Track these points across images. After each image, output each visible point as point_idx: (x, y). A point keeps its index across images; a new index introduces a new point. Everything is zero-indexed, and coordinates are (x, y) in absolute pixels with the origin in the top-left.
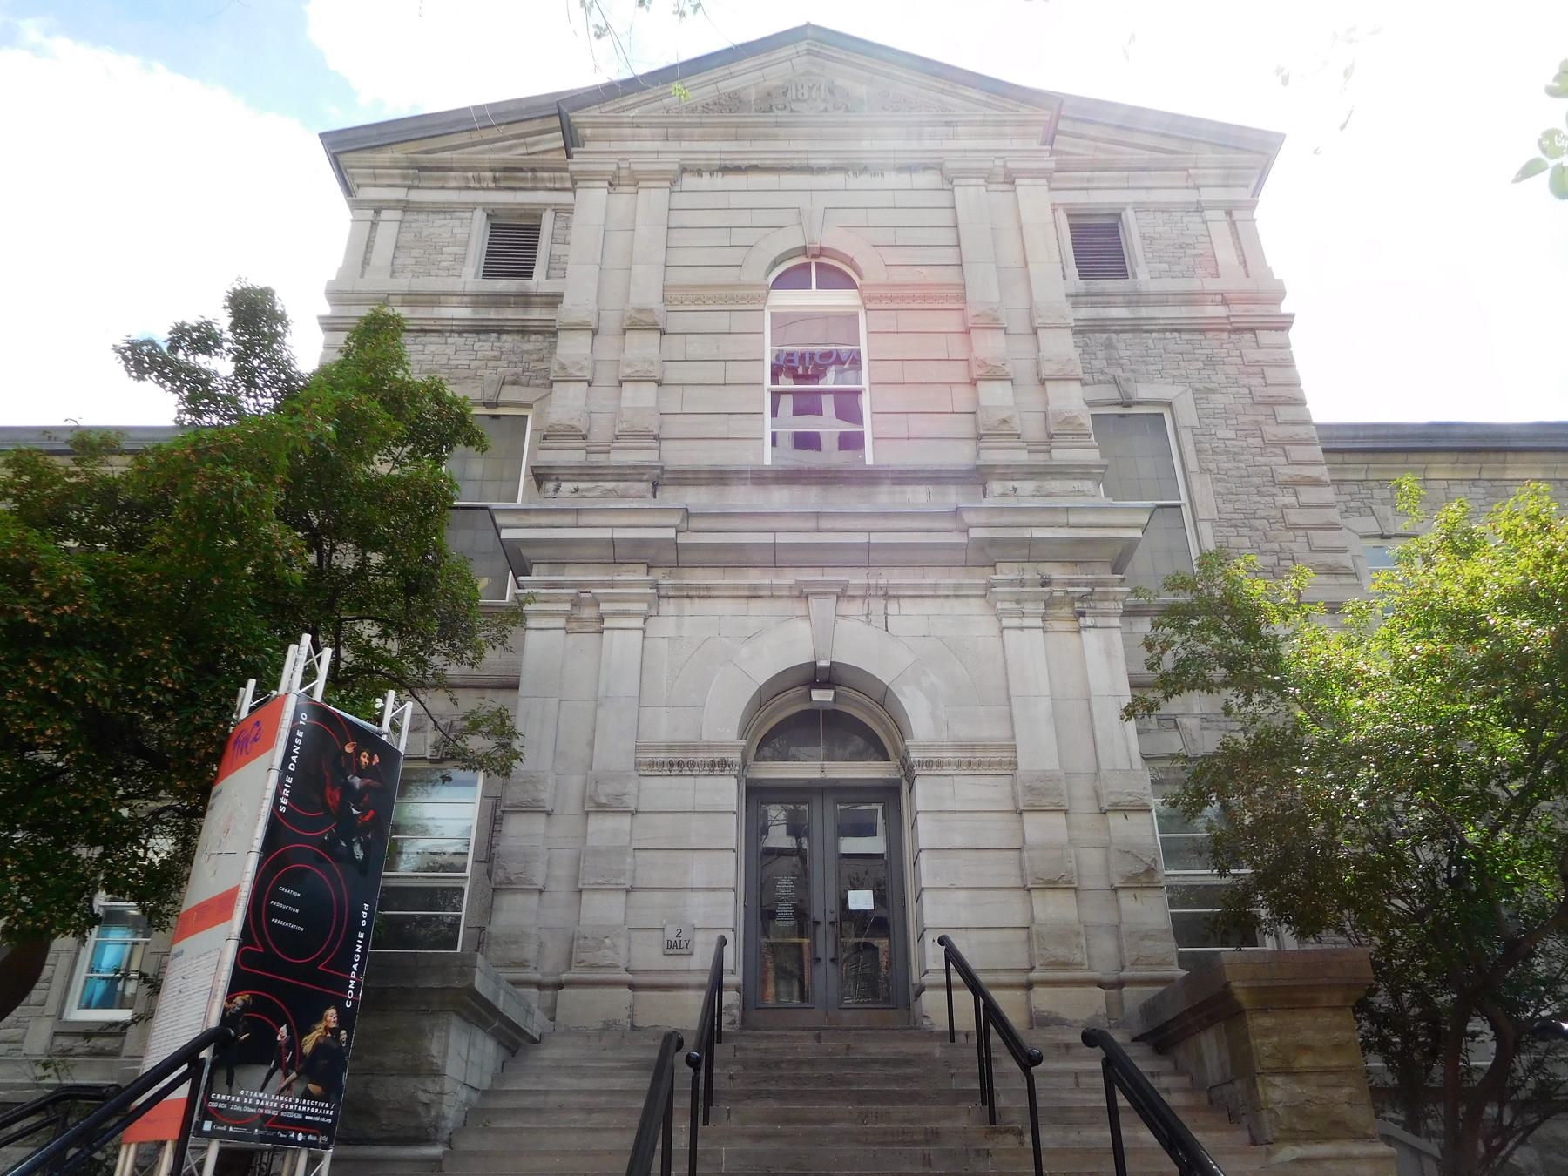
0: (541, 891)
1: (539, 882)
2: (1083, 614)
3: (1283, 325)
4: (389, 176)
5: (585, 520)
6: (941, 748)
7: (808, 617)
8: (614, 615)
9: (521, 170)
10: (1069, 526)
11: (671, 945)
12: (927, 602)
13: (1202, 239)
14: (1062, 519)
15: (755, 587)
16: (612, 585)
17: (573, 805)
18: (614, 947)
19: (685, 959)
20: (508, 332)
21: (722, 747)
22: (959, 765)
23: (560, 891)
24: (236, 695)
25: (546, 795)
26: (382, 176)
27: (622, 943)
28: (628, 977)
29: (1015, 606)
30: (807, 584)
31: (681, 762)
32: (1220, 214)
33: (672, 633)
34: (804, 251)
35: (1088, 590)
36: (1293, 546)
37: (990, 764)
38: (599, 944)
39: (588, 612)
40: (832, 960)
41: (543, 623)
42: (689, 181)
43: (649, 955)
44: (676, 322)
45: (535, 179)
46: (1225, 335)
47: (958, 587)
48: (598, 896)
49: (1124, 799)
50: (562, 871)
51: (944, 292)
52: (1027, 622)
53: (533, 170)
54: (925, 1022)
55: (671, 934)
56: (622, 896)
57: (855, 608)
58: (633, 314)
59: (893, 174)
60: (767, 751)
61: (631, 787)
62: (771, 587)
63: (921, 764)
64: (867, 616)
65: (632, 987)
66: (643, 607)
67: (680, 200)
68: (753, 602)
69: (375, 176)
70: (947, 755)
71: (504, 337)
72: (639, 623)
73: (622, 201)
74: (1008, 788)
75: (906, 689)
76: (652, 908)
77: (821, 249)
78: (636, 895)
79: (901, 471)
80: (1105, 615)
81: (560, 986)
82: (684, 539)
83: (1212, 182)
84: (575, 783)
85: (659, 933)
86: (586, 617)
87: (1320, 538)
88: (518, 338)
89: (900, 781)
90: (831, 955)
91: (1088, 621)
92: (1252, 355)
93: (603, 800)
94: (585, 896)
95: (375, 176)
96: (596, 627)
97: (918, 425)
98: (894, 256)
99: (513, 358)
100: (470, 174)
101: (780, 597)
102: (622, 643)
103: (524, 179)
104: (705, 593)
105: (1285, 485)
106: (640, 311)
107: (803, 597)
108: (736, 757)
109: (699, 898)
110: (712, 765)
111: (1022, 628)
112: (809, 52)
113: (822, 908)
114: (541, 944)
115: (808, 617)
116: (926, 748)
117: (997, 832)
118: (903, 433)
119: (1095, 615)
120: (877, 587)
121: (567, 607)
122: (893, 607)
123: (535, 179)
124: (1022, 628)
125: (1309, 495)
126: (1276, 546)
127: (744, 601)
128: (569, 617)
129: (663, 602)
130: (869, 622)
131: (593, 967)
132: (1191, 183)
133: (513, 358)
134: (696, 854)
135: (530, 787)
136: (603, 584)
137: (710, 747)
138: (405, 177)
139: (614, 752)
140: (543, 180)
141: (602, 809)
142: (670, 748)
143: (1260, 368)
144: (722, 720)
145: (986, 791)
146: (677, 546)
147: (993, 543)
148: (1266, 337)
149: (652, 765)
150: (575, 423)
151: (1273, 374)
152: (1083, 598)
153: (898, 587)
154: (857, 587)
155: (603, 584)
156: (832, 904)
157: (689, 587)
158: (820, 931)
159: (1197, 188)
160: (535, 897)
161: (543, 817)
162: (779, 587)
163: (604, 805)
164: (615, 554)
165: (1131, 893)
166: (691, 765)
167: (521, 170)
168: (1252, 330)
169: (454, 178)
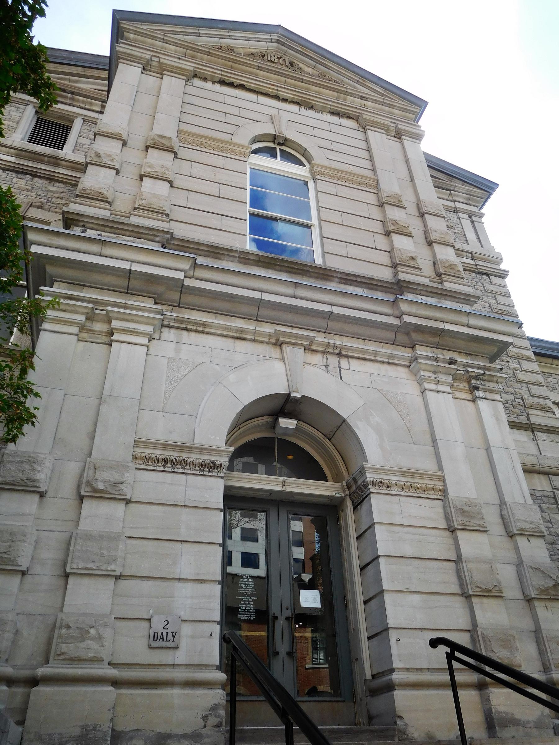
0: (24, 573)
1: (24, 563)
2: (477, 388)
3: (503, 275)
5: (108, 251)
6: (390, 472)
7: (283, 360)
8: (124, 331)
10: (468, 326)
11: (157, 637)
12: (368, 364)
13: (458, 226)
14: (464, 320)
15: (242, 331)
16: (125, 306)
17: (68, 489)
18: (99, 638)
19: (171, 652)
20: (40, 177)
21: (213, 451)
22: (403, 488)
23: (45, 576)
25: (42, 476)
27: (107, 633)
28: (113, 672)
29: (433, 375)
30: (284, 334)
31: (174, 460)
32: (466, 216)
33: (172, 354)
34: (274, 138)
35: (481, 372)
36: (521, 391)
37: (426, 490)
38: (83, 634)
39: (99, 326)
40: (289, 654)
41: (57, 328)
42: (197, 82)
43: (130, 646)
44: (182, 153)
46: (474, 274)
47: (392, 356)
48: (86, 581)
49: (527, 526)
50: (50, 554)
51: (365, 181)
52: (441, 388)
53: (72, 93)
54: (399, 722)
55: (158, 625)
56: (112, 581)
57: (317, 359)
58: (156, 138)
59: (329, 115)
60: (238, 463)
61: (129, 476)
62: (255, 333)
63: (374, 483)
64: (326, 366)
65: (116, 683)
66: (150, 329)
67: (189, 89)
68: (239, 343)
70: (394, 478)
71: (36, 179)
72: (145, 341)
73: (151, 80)
74: (441, 510)
75: (360, 424)
76: (140, 597)
77: (286, 139)
78: (123, 583)
79: (347, 274)
80: (491, 391)
81: (34, 682)
82: (188, 282)
83: (461, 200)
84: (72, 469)
85: (146, 624)
86: (101, 330)
87: (535, 390)
88: (46, 182)
89: (342, 501)
90: (287, 649)
91: (479, 394)
92: (489, 287)
93: (101, 486)
94: (71, 580)
96: (105, 339)
97: (353, 251)
98: (331, 155)
99: (41, 193)
101: (260, 342)
102: (128, 355)
104: (201, 329)
105: (513, 357)
106: (162, 137)
107: (279, 344)
108: (225, 460)
109: (187, 589)
110: (203, 465)
111: (438, 392)
112: (278, 42)
113: (278, 607)
114: (17, 632)
115: (283, 360)
116: (376, 470)
117: (438, 545)
118: (344, 253)
119: (485, 390)
120: (335, 347)
121: (83, 318)
122: (344, 363)
123: (72, 99)
124: (438, 392)
125: (526, 365)
126: (512, 390)
127: (231, 340)
128: (82, 328)
129: (165, 330)
130: (328, 371)
131: (74, 660)
132: (451, 198)
133: (41, 193)
134: (185, 545)
135: (27, 466)
136: (116, 305)
137: (202, 450)
139: (113, 445)
140: (78, 101)
141: (98, 495)
142: (166, 446)
143: (494, 295)
144: (213, 432)
145: (429, 512)
146: (182, 288)
147: (418, 328)
148: (495, 280)
149: (147, 460)
150: (104, 192)
151: (500, 299)
152: (477, 378)
153: (349, 348)
154: (320, 344)
155: (116, 305)
156: (287, 602)
157: (188, 321)
158: (278, 625)
159: (454, 201)
160: (17, 579)
161: (36, 497)
162: (261, 334)
163: (101, 491)
164: (131, 284)
165: (542, 604)
166: (183, 463)
167: (64, 91)
168: (487, 275)
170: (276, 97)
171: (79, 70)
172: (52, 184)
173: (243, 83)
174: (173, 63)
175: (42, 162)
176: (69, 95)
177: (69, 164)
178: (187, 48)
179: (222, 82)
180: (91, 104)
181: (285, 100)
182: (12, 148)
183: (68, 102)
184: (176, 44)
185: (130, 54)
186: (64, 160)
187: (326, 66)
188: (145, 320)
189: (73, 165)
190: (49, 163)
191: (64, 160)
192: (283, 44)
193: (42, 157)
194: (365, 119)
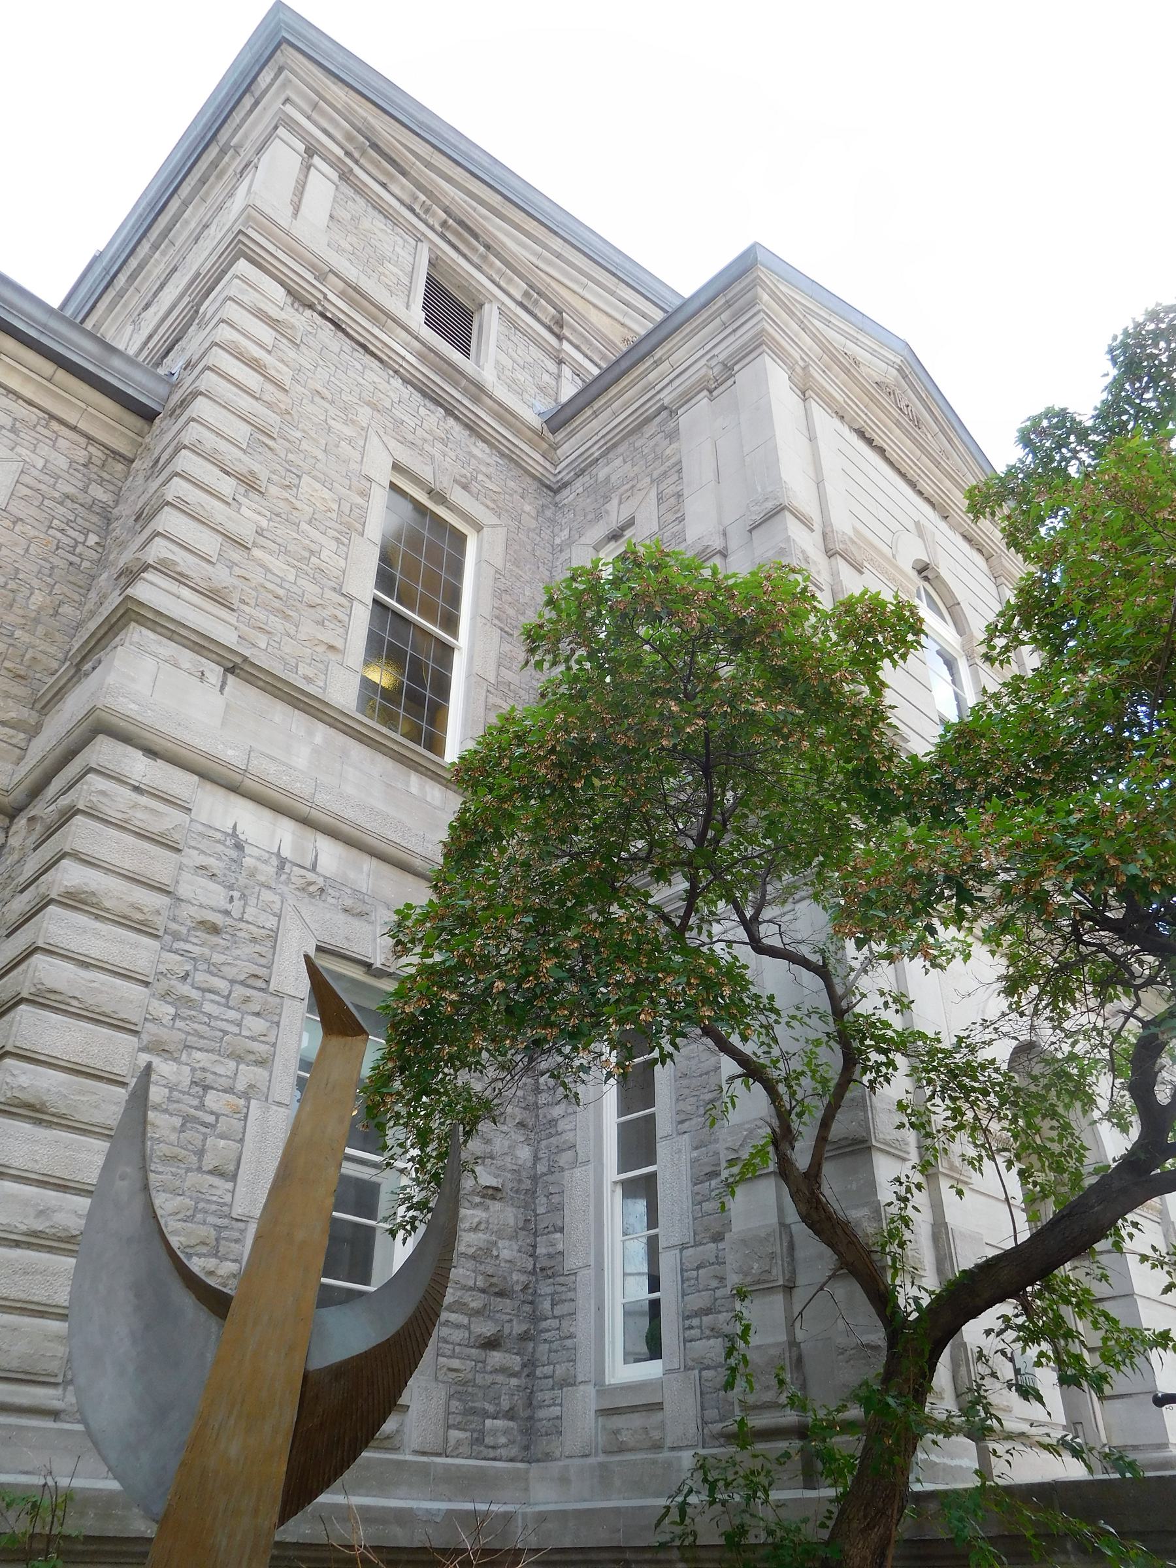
4: (332, 120)
9: (476, 236)
20: (457, 418)
24: (497, 1515)
26: (323, 113)
45: (484, 258)
69: (315, 106)
77: (938, 577)
95: (315, 106)
100: (423, 197)
103: (475, 250)
112: (900, 370)
123: (484, 258)
138: (349, 138)
140: (491, 265)
167: (476, 236)
169: (402, 186)
170: (913, 485)
171: (495, 200)
172: (473, 439)
173: (886, 447)
174: (825, 384)
175: (455, 385)
176: (482, 249)
177: (496, 406)
178: (826, 350)
179: (861, 434)
180: (510, 281)
181: (920, 493)
182: (416, 338)
183: (475, 259)
184: (814, 338)
185: (773, 338)
186: (490, 397)
187: (950, 441)
188: (261, 684)
189: (501, 411)
190: (465, 392)
191: (490, 397)
192: (905, 377)
193: (458, 376)
194: (1003, 566)
